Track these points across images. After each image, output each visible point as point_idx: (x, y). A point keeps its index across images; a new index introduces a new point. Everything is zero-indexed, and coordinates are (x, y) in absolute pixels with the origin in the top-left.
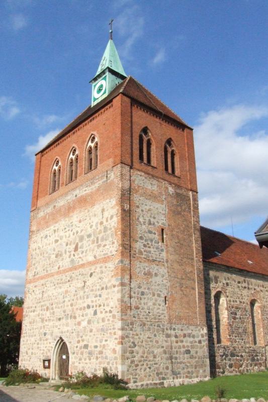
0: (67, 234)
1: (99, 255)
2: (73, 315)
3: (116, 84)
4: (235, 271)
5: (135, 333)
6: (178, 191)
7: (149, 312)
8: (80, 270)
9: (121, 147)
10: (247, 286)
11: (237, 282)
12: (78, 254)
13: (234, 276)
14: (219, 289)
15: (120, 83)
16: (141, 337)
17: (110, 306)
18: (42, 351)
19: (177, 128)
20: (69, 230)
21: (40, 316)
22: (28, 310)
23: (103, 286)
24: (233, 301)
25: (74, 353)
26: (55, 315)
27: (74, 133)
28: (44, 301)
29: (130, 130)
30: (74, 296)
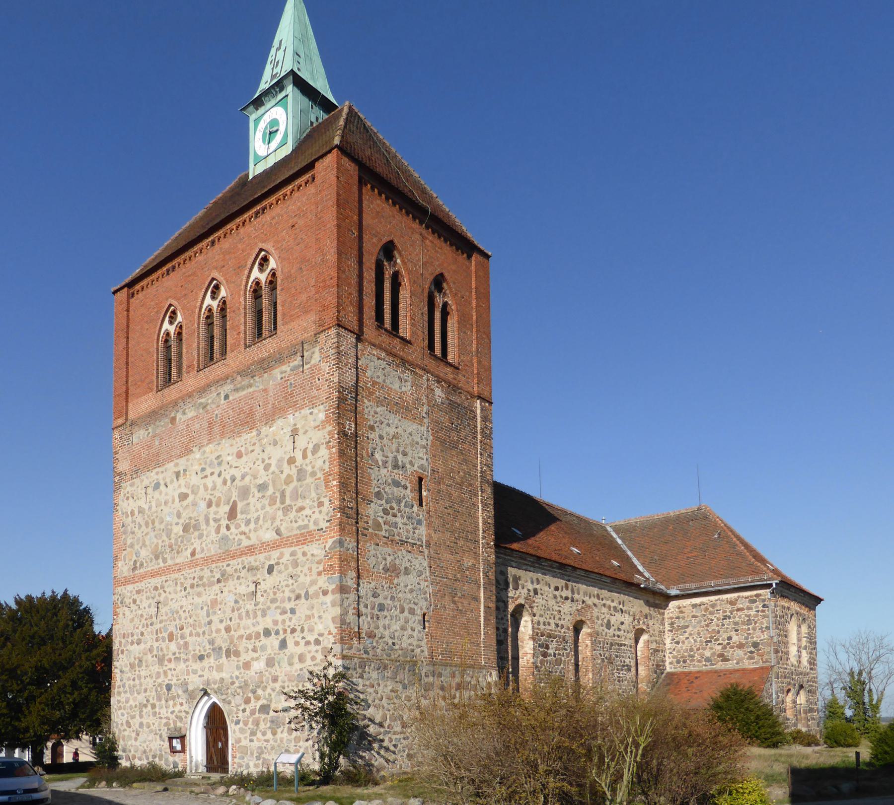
0: (209, 482)
2: (232, 649)
3: (312, 123)
4: (551, 566)
7: (394, 644)
8: (244, 558)
9: (338, 286)
10: (570, 595)
11: (552, 588)
12: (238, 526)
13: (548, 578)
14: (521, 601)
15: (320, 120)
16: (380, 689)
17: (316, 632)
18: (164, 721)
20: (212, 474)
21: (155, 653)
22: (123, 641)
25: (237, 723)
26: (190, 648)
28: (161, 622)
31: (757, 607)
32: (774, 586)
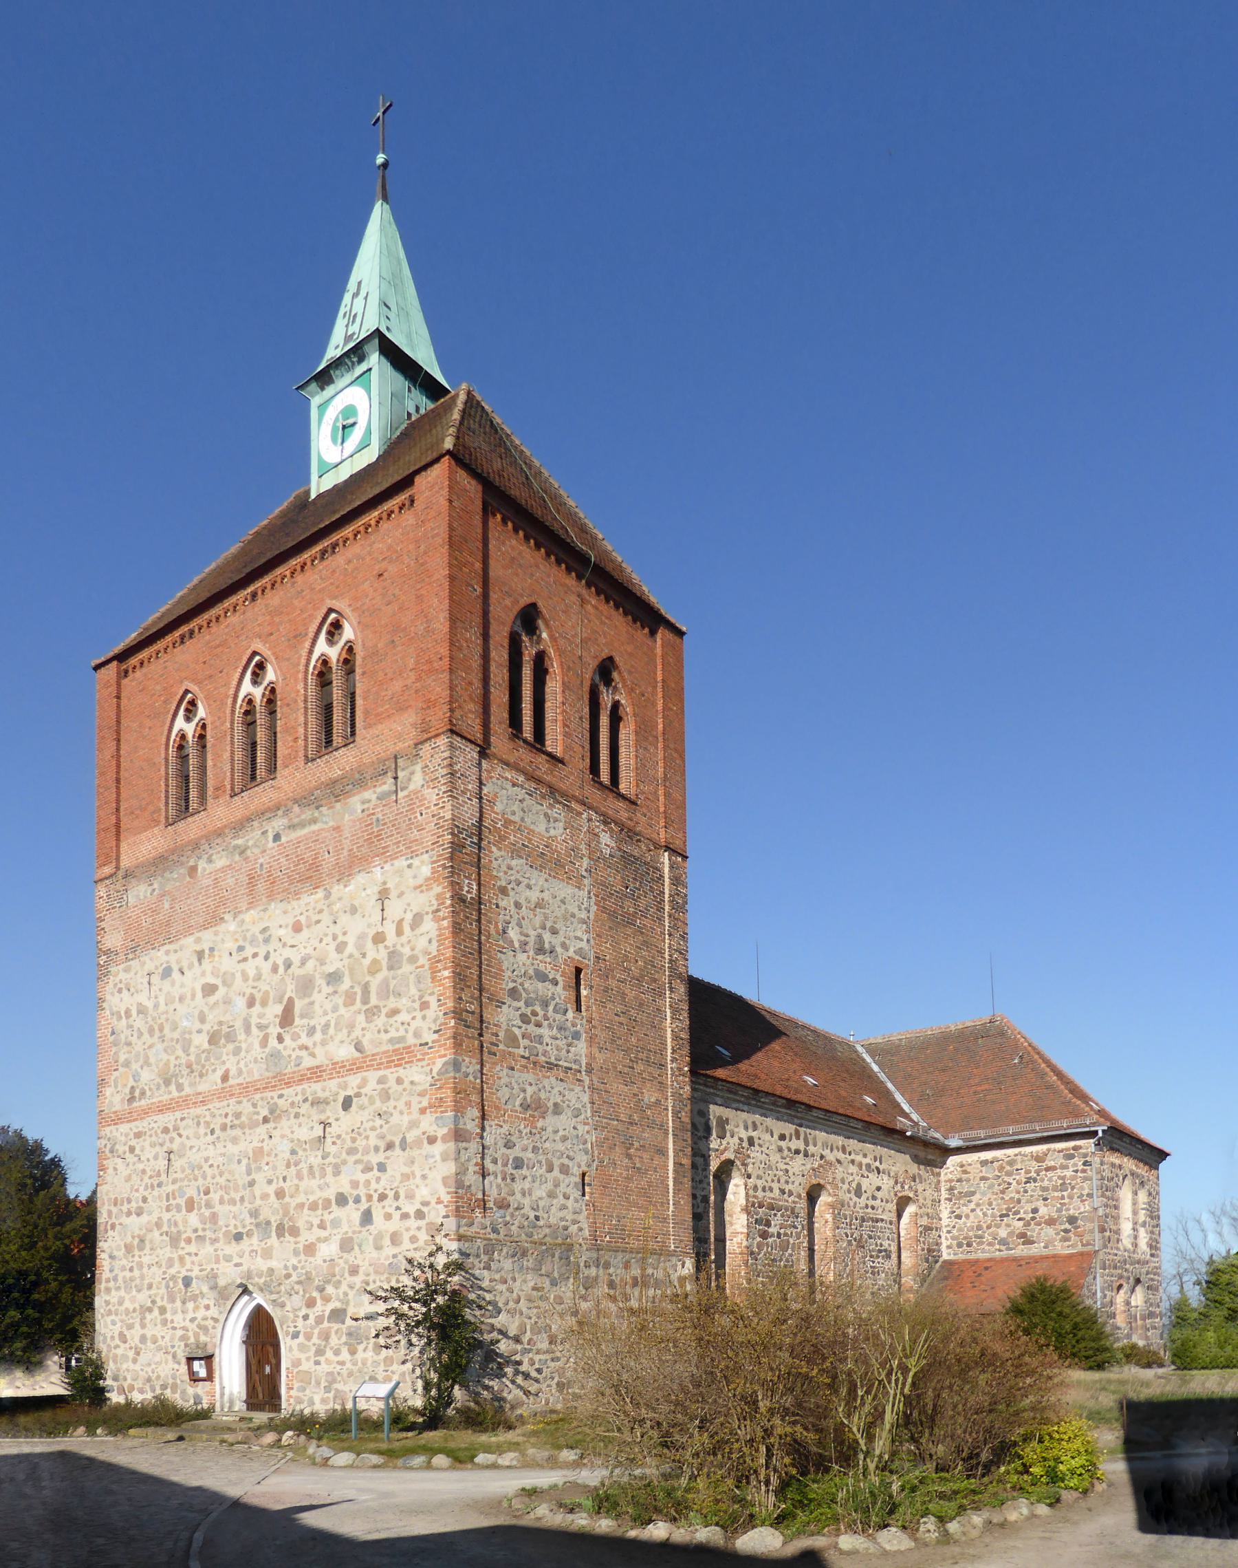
0: (250, 968)
1: (372, 1041)
3: (409, 415)
4: (774, 1104)
5: (497, 1277)
6: (628, 848)
7: (537, 1218)
10: (802, 1148)
11: (776, 1137)
12: (295, 1037)
14: (729, 1155)
15: (422, 411)
18: (180, 1333)
19: (635, 621)
20: (255, 955)
21: (165, 1228)
23: (389, 1138)
24: (764, 1190)
25: (295, 1335)
27: (254, 596)
28: (174, 1182)
29: (478, 607)
30: (288, 1166)
31: (1075, 1165)
32: (1100, 1134)
